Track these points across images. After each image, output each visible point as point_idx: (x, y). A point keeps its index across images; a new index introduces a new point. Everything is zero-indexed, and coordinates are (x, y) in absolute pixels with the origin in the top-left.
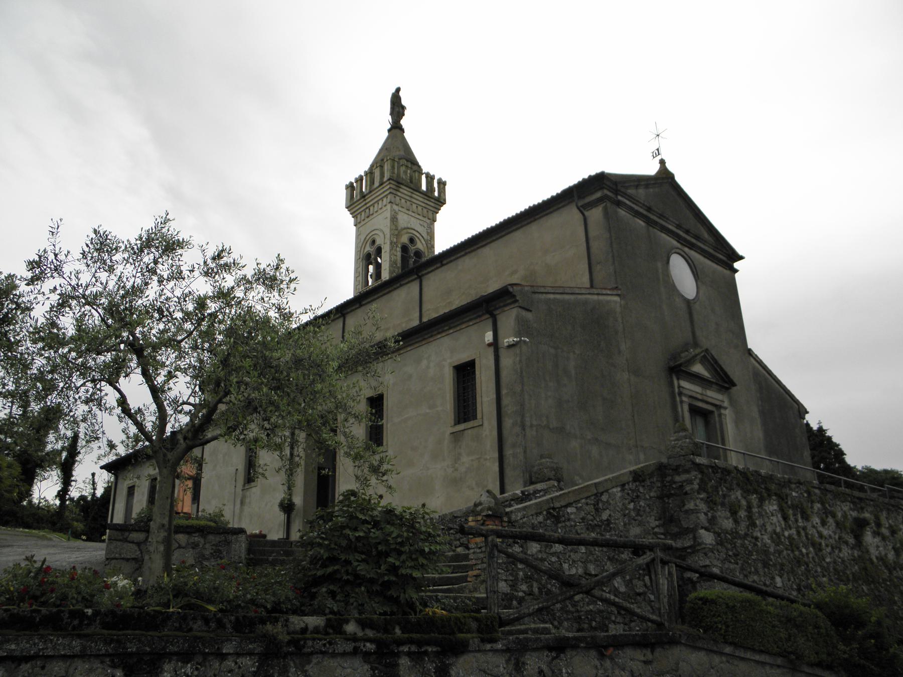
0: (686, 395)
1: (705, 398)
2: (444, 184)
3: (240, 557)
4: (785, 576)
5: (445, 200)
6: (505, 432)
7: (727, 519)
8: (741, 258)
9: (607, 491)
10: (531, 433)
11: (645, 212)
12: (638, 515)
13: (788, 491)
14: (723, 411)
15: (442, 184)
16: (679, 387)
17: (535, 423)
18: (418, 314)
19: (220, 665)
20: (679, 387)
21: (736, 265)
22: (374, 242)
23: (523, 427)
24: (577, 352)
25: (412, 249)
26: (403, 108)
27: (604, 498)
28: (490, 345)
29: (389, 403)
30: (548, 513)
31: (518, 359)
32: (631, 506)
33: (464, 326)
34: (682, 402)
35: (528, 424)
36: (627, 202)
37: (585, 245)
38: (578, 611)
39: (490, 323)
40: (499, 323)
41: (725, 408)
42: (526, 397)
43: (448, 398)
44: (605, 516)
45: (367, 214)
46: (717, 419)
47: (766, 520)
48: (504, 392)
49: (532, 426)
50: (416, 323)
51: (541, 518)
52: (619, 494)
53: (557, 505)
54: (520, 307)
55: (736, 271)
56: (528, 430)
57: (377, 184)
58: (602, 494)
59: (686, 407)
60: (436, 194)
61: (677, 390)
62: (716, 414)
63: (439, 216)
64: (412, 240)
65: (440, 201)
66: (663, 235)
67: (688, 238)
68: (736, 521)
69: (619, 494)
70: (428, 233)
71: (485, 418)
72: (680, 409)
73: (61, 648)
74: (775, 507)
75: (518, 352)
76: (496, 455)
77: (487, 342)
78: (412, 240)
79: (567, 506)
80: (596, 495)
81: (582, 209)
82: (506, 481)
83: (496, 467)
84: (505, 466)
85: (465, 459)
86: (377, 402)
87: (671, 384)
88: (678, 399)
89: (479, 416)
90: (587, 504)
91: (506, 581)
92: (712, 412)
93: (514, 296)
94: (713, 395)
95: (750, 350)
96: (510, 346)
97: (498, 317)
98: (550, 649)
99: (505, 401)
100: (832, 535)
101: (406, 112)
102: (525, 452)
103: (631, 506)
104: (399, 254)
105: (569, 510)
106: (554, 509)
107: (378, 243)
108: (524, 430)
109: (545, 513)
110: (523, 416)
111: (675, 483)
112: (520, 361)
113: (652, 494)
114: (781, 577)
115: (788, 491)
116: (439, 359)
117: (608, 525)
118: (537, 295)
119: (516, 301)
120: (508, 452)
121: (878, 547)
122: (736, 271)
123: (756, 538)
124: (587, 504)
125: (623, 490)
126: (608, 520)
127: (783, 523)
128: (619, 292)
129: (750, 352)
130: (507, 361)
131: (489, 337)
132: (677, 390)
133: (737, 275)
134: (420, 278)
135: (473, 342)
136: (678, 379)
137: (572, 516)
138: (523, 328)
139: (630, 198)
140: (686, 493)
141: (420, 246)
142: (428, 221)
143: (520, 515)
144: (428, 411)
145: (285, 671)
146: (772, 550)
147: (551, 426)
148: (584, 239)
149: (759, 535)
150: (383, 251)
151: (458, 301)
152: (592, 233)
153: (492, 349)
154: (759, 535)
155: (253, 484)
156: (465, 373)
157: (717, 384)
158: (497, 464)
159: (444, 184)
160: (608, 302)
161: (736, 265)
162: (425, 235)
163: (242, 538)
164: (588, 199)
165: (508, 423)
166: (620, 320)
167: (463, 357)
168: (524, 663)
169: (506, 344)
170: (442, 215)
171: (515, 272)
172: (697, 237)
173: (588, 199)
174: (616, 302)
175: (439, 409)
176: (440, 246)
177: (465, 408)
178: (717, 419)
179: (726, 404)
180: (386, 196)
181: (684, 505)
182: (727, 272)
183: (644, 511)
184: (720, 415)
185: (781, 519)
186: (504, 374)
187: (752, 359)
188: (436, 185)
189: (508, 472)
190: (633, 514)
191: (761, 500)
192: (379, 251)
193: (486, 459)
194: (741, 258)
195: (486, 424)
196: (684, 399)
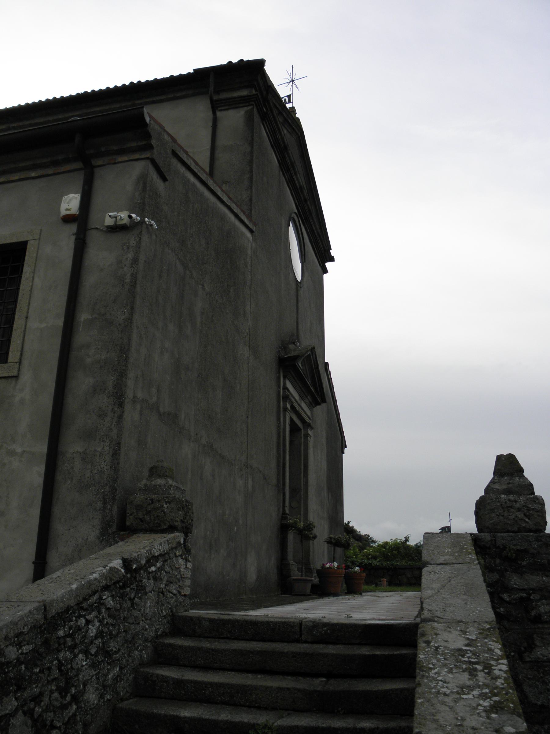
6: (72, 404)
10: (131, 414)
17: (140, 395)
21: (328, 265)
23: (119, 399)
24: (207, 289)
28: (68, 219)
31: (130, 255)
33: (16, 177)
35: (130, 394)
37: (208, 154)
39: (79, 179)
40: (98, 184)
42: (135, 337)
48: (83, 316)
49: (135, 400)
54: (153, 162)
56: (128, 407)
62: (303, 432)
71: (25, 363)
75: (133, 242)
76: (43, 448)
77: (63, 212)
81: (215, 106)
82: (57, 511)
83: (36, 475)
84: (59, 477)
89: (13, 356)
93: (148, 136)
96: (117, 229)
97: (98, 172)
99: (81, 337)
102: (116, 454)
108: (121, 405)
110: (122, 375)
111: (508, 589)
112: (135, 261)
118: (174, 161)
119: (150, 147)
120: (72, 447)
128: (254, 229)
130: (102, 256)
131: (71, 203)
133: (325, 276)
136: (285, 377)
138: (145, 201)
140: (538, 619)
147: (162, 410)
148: (208, 146)
152: (222, 141)
153: (73, 228)
158: (42, 469)
160: (243, 234)
161: (328, 265)
164: (224, 96)
165: (81, 383)
166: (249, 267)
169: (109, 222)
173: (224, 96)
181: (531, 647)
182: (320, 269)
184: (307, 435)
186: (90, 279)
189: (65, 491)
193: (12, 453)
195: (26, 376)
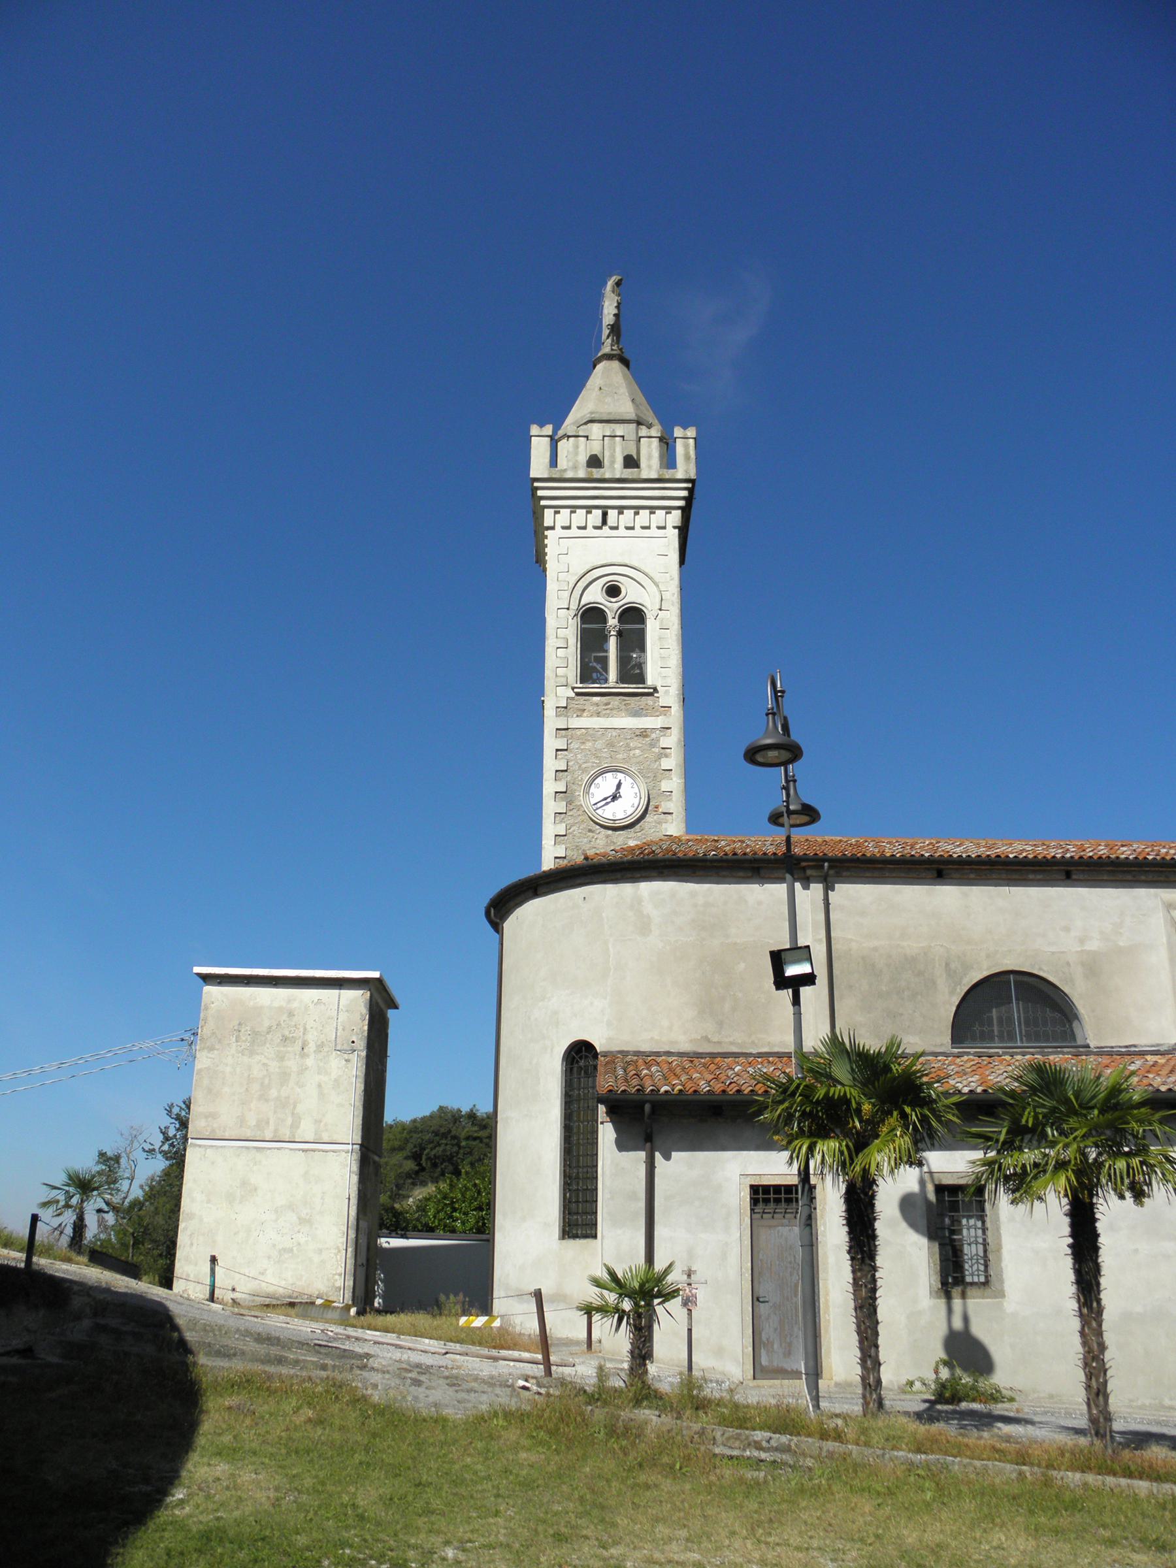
22: (613, 591)
180: (652, 510)
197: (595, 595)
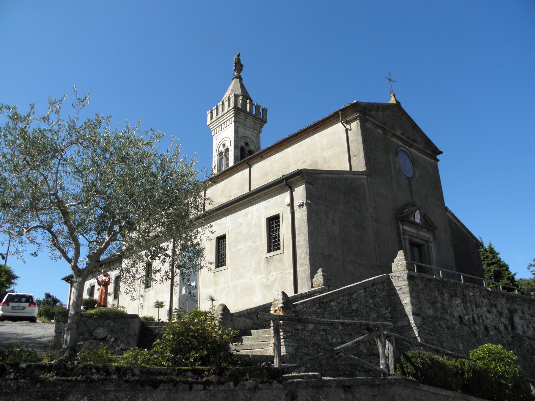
0: (407, 235)
1: (419, 236)
2: (266, 110)
3: (135, 332)
4: (465, 343)
5: (266, 120)
7: (429, 309)
8: (441, 153)
9: (356, 292)
11: (382, 126)
12: (375, 306)
13: (467, 292)
14: (429, 244)
15: (265, 110)
16: (403, 229)
18: (248, 187)
19: (105, 397)
20: (403, 229)
21: (438, 157)
22: (224, 145)
25: (247, 149)
26: (242, 66)
27: (354, 296)
29: (229, 241)
30: (319, 305)
32: (371, 301)
34: (404, 239)
36: (371, 119)
38: (337, 365)
41: (432, 242)
43: (264, 237)
44: (354, 307)
45: (225, 126)
46: (426, 249)
47: (454, 309)
50: (247, 191)
51: (314, 309)
52: (363, 294)
53: (325, 301)
55: (438, 160)
57: (226, 111)
58: (352, 294)
59: (407, 242)
60: (261, 116)
61: (401, 231)
63: (263, 130)
64: (247, 144)
65: (264, 121)
66: (394, 139)
67: (409, 141)
68: (436, 310)
69: (363, 294)
70: (256, 140)
72: (403, 243)
73: (4, 388)
74: (459, 302)
77: (287, 204)
78: (247, 144)
79: (330, 301)
80: (349, 294)
85: (274, 273)
86: (221, 241)
87: (398, 228)
88: (402, 237)
90: (343, 300)
91: (292, 346)
92: (423, 245)
94: (424, 234)
95: (446, 208)
98: (312, 387)
100: (495, 319)
101: (243, 68)
103: (371, 301)
104: (239, 152)
105: (332, 303)
106: (323, 303)
107: (226, 146)
109: (317, 305)
113: (384, 294)
114: (462, 344)
115: (467, 292)
116: (259, 212)
117: (356, 313)
121: (523, 326)
122: (438, 160)
123: (448, 320)
124: (343, 300)
125: (365, 292)
126: (356, 310)
127: (464, 311)
129: (446, 209)
131: (288, 201)
132: (401, 231)
133: (438, 163)
134: (250, 167)
135: (278, 204)
136: (402, 225)
137: (334, 307)
139: (373, 117)
141: (252, 147)
142: (257, 132)
143: (302, 306)
144: (251, 245)
145: (145, 399)
146: (457, 328)
149: (449, 318)
150: (230, 150)
151: (271, 179)
153: (289, 208)
154: (449, 318)
155: (149, 289)
156: (273, 222)
157: (425, 228)
159: (266, 110)
161: (438, 157)
162: (255, 141)
163: (137, 320)
167: (272, 213)
168: (296, 396)
170: (265, 128)
171: (305, 162)
172: (414, 141)
174: (364, 179)
175: (259, 243)
176: (263, 147)
177: (273, 244)
178: (426, 249)
179: (432, 240)
180: (229, 120)
182: (432, 161)
183: (379, 304)
184: (428, 247)
185: (463, 309)
187: (448, 213)
188: (261, 111)
190: (372, 306)
191: (452, 297)
192: (227, 150)
193: (286, 273)
194: (441, 153)
196: (406, 237)
197: (222, 149)
